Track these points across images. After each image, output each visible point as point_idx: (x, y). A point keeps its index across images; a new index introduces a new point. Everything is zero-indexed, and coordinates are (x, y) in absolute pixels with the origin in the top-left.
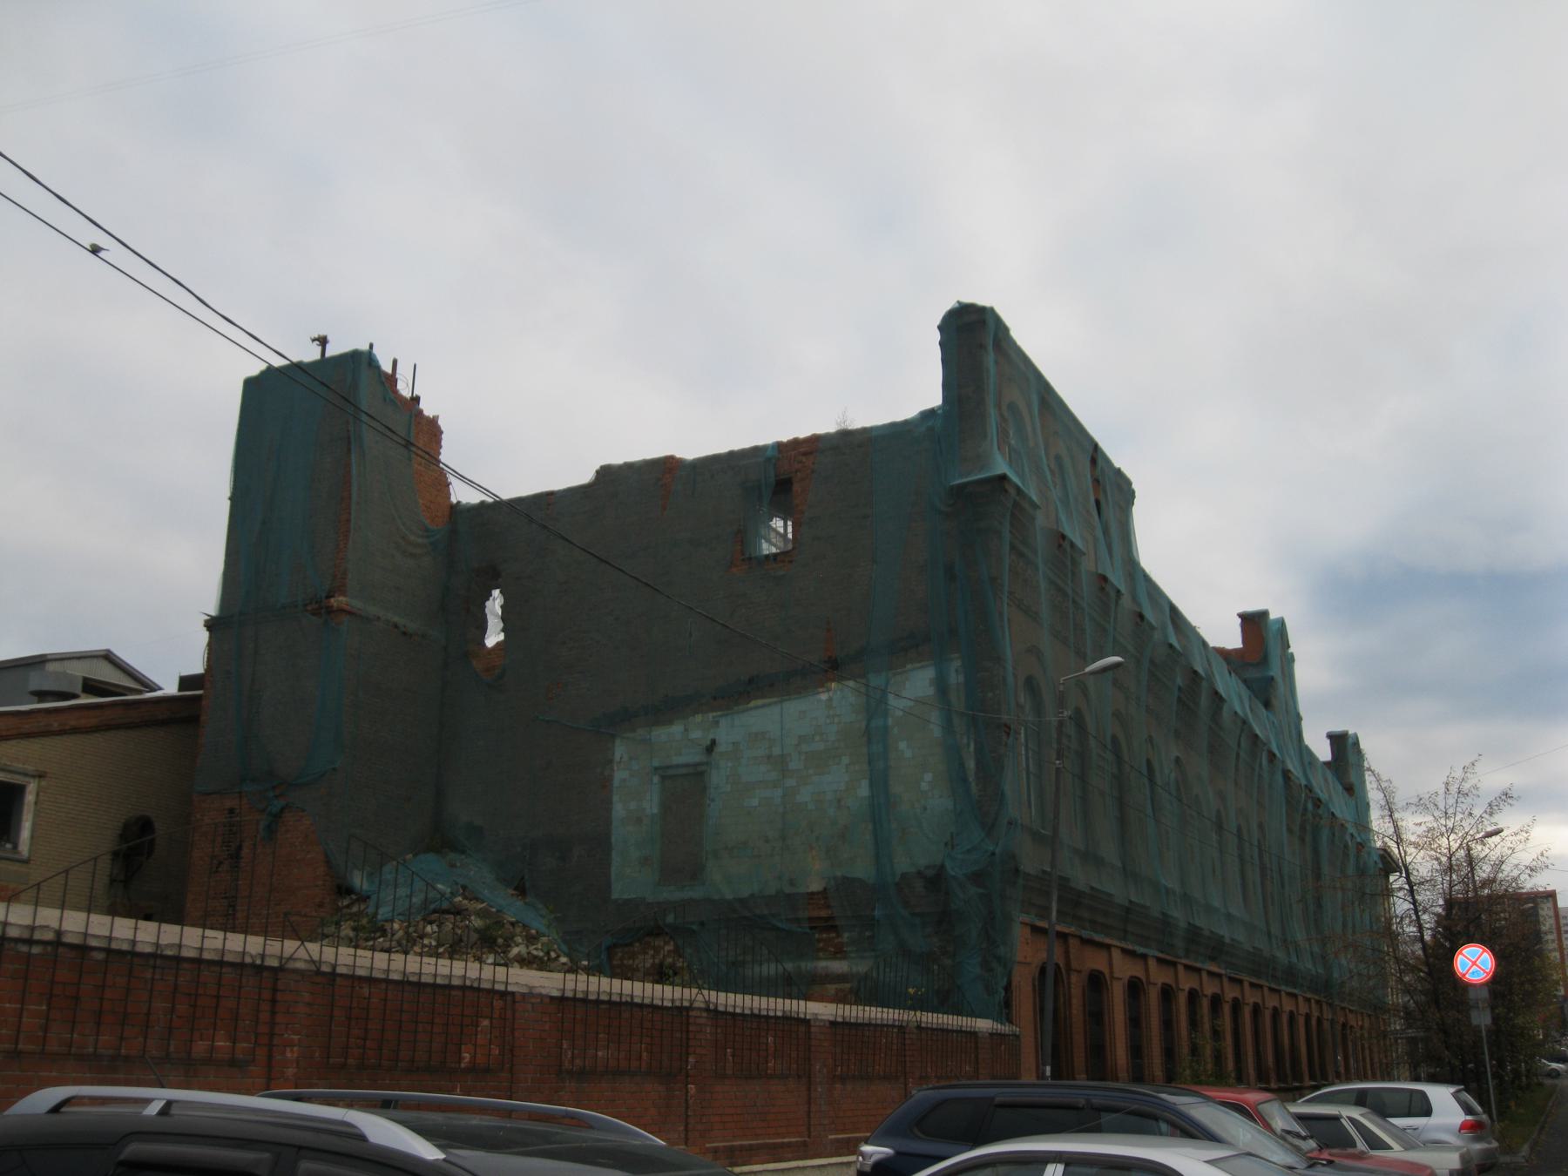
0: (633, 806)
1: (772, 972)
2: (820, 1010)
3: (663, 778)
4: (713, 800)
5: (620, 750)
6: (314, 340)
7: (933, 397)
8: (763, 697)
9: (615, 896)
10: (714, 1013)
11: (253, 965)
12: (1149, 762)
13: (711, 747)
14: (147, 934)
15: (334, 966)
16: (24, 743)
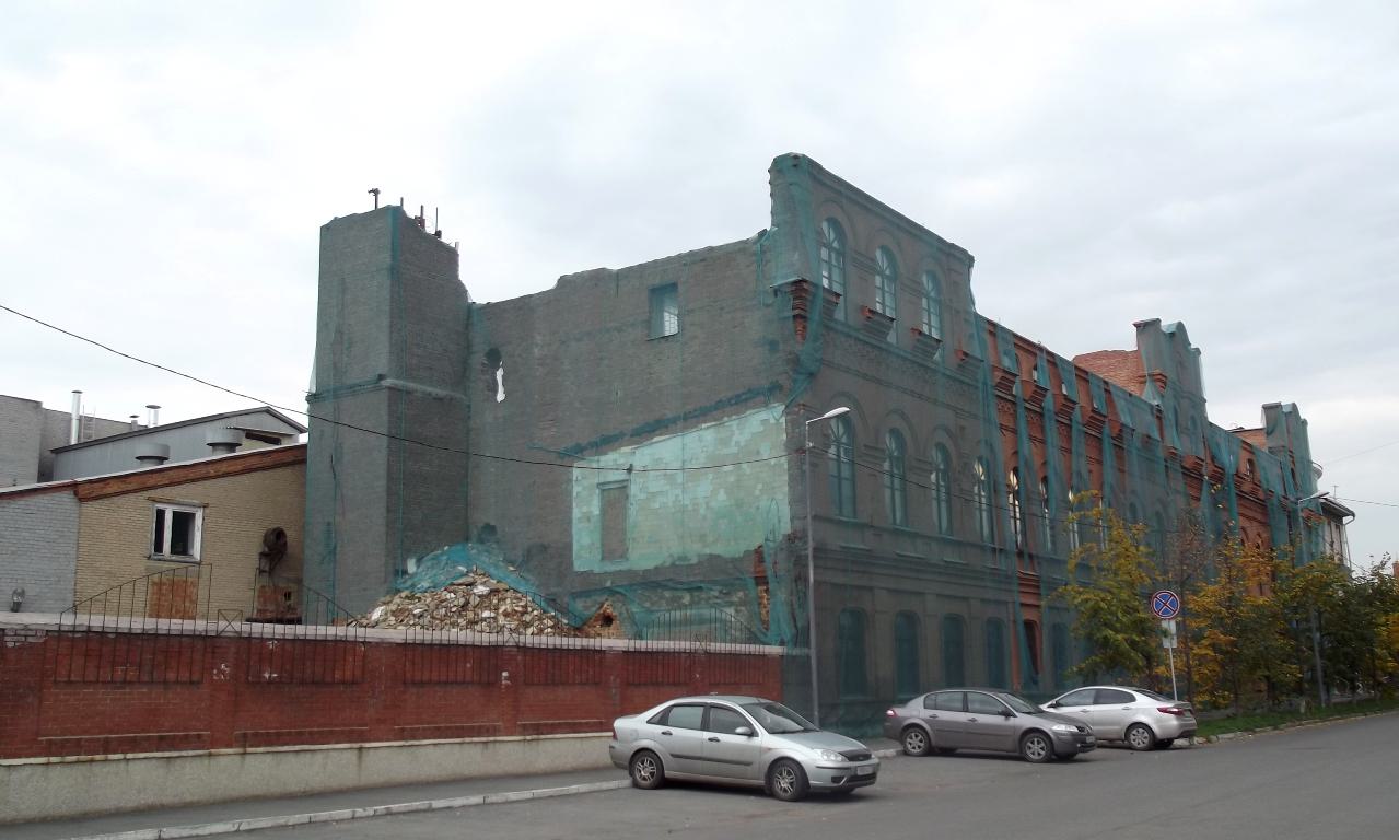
0: (585, 509)
1: (678, 616)
3: (603, 490)
4: (632, 504)
5: (576, 473)
7: (766, 223)
8: (661, 435)
9: (579, 566)
11: (200, 636)
12: (1193, 418)
15: (250, 634)
16: (192, 485)
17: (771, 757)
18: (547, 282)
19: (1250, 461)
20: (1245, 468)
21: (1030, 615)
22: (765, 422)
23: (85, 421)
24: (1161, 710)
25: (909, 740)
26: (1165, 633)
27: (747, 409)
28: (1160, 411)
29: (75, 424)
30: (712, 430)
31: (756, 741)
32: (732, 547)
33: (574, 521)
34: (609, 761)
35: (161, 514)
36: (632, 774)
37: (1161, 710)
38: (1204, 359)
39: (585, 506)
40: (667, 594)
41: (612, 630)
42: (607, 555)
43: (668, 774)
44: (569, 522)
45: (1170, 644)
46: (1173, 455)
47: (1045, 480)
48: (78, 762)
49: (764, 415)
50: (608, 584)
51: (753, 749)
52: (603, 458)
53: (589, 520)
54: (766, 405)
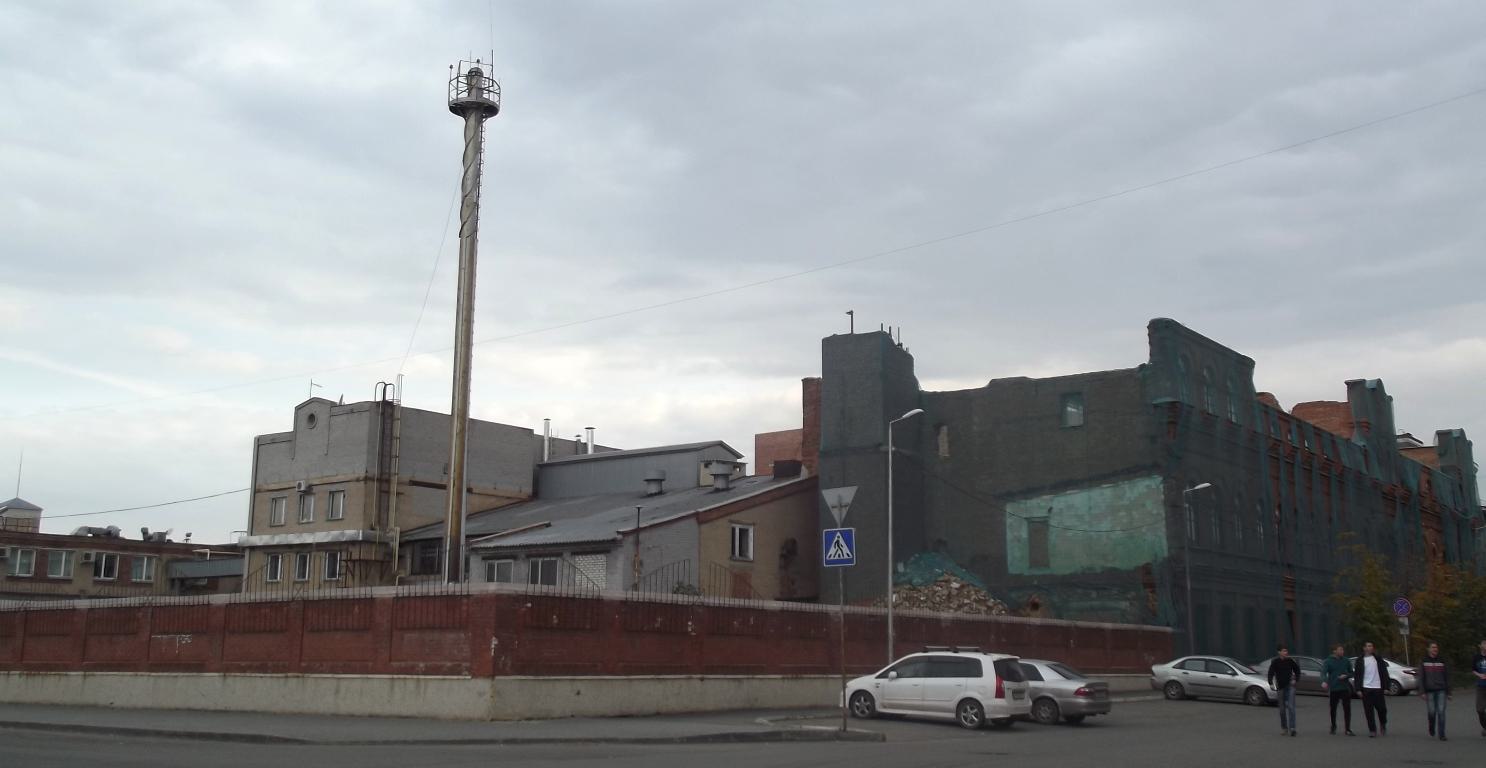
2: (1108, 625)
6: (475, 74)
7: (1145, 359)
9: (1012, 570)
10: (1077, 627)
13: (1050, 510)
14: (1016, 619)
17: (1247, 685)
18: (982, 383)
19: (1429, 482)
20: (1425, 487)
21: (1289, 607)
22: (1148, 486)
23: (597, 448)
24: (1405, 672)
25: (963, 714)
26: (1402, 625)
27: (1136, 477)
28: (1366, 451)
29: (546, 443)
30: (1109, 490)
31: (1236, 678)
32: (1126, 561)
33: (1009, 542)
34: (1150, 687)
35: (734, 530)
36: (1165, 693)
37: (1405, 672)
38: (1395, 404)
39: (1016, 533)
40: (1080, 591)
41: (1038, 612)
42: (1034, 562)
43: (1188, 692)
44: (1005, 540)
45: (1404, 632)
46: (1376, 484)
47: (1279, 507)
48: (652, 679)
49: (1147, 482)
50: (1035, 583)
51: (1237, 681)
52: (1028, 501)
53: (1019, 541)
54: (1149, 475)
